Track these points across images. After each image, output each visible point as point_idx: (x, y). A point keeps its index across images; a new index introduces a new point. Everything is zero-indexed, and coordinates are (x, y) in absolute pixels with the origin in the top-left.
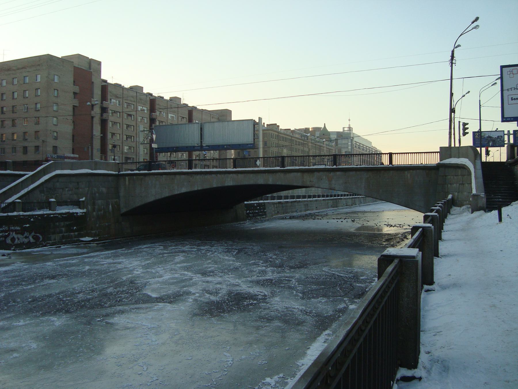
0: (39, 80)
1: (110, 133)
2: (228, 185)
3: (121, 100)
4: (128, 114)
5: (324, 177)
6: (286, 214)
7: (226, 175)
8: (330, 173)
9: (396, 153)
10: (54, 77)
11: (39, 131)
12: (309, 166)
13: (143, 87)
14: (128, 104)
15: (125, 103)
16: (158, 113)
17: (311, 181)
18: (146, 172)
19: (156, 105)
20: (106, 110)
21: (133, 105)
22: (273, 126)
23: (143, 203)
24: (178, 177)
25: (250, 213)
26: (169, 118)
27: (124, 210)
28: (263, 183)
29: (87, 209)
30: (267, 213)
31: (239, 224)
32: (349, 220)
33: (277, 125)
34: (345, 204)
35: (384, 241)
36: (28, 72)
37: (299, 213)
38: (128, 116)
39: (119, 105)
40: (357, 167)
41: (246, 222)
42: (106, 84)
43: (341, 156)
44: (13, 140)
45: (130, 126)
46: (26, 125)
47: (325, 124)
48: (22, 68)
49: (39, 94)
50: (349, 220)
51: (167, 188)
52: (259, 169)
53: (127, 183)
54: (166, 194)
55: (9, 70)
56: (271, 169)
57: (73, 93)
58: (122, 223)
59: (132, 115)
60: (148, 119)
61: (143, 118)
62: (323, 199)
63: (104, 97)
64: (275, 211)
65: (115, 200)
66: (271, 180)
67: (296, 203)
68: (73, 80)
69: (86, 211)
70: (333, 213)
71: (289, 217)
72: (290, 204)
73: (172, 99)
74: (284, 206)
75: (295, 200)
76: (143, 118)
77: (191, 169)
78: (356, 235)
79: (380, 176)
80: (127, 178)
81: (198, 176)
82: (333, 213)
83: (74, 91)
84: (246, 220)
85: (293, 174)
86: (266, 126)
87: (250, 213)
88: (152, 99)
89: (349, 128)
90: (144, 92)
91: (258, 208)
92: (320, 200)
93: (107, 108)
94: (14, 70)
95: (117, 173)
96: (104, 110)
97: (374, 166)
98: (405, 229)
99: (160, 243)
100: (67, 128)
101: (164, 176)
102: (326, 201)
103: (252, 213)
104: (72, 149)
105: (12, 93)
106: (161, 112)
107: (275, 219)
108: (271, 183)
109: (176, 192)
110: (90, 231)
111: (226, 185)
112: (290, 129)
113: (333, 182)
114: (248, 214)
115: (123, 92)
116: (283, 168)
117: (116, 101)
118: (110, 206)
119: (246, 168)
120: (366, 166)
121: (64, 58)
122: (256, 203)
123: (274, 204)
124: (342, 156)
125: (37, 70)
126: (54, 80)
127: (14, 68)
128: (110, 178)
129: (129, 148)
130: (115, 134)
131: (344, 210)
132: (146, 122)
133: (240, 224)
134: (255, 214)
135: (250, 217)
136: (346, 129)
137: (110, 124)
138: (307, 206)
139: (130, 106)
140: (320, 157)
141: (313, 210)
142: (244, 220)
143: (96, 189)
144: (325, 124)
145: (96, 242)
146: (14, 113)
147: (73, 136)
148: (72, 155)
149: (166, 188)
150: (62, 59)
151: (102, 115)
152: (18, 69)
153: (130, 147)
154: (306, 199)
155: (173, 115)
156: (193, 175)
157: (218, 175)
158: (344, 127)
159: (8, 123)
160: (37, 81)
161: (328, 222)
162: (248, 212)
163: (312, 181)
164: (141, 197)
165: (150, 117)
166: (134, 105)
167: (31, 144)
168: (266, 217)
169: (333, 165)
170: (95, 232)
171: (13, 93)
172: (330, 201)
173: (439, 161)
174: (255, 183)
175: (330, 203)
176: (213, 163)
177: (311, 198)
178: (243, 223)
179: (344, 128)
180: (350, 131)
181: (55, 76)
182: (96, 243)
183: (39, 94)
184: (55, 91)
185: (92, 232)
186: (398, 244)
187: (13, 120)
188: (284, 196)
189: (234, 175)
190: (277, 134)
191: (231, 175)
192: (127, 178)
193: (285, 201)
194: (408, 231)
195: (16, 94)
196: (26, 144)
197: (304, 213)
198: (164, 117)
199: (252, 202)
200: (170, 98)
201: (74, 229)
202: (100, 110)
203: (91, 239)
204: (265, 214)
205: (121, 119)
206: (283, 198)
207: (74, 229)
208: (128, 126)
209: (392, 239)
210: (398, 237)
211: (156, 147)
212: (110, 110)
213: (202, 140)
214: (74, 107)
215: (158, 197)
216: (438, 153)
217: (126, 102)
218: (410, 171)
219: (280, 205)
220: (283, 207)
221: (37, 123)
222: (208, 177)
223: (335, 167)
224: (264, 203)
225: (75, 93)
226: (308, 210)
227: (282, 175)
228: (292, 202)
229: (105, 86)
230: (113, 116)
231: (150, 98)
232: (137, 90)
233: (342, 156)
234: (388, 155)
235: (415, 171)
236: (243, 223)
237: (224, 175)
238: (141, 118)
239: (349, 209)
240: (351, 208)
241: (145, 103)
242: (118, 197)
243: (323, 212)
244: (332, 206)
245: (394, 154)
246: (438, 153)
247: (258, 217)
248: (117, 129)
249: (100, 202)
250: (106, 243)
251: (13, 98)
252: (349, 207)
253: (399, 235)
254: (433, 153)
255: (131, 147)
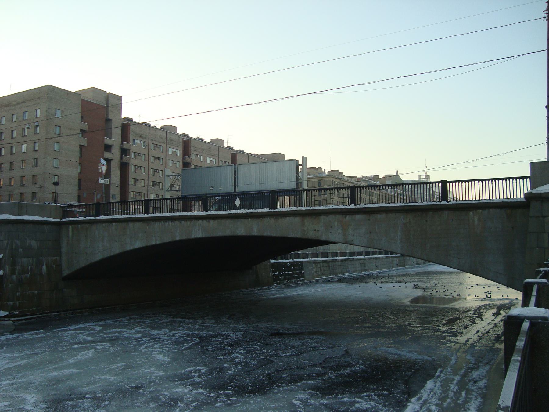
0: (38, 115)
1: (132, 178)
2: (196, 237)
3: (147, 141)
4: (155, 157)
5: (336, 223)
6: (335, 275)
7: (194, 222)
8: (345, 217)
9: (452, 182)
10: (56, 112)
11: (37, 175)
12: (312, 206)
13: (176, 127)
14: (156, 146)
15: (152, 145)
16: (193, 157)
17: (315, 230)
18: (93, 218)
19: (191, 147)
20: (128, 151)
21: (161, 147)
22: (335, 172)
23: (88, 263)
24: (131, 225)
25: (279, 275)
26: (208, 162)
27: (66, 273)
28: (244, 234)
29: (4, 270)
30: (305, 274)
31: (260, 289)
32: (410, 285)
33: (340, 171)
34: (415, 262)
35: (444, 325)
36: (28, 106)
37: (353, 275)
38: (155, 159)
39: (144, 146)
40: (388, 207)
41: (271, 287)
42: (188, 139)
43: (363, 189)
44: (11, 186)
45: (158, 171)
46: (24, 168)
47: (397, 171)
48: (24, 102)
49: (38, 132)
50: (410, 285)
51: (117, 241)
52: (239, 212)
53: (70, 234)
54: (116, 250)
55: (9, 105)
56: (255, 211)
57: (80, 130)
58: (65, 290)
59: (160, 158)
60: (181, 163)
61: (174, 162)
62: (387, 257)
63: (125, 137)
64: (318, 271)
65: (54, 258)
66: (255, 229)
67: (349, 262)
68: (80, 116)
69: (3, 273)
70: (397, 273)
71: (336, 280)
72: (340, 263)
73: (213, 141)
74: (330, 266)
75: (346, 258)
76: (174, 162)
77: (148, 214)
78: (406, 310)
79: (427, 221)
80: (70, 227)
81: (157, 224)
82: (397, 273)
83: (81, 129)
84: (271, 284)
85: (288, 220)
86: (326, 172)
87: (281, 276)
88: (185, 140)
89: (426, 175)
90: (178, 132)
91: (292, 268)
92: (382, 258)
93: (129, 150)
94: (14, 105)
95: (59, 220)
96: (124, 152)
97: (417, 204)
98: (482, 300)
99: (111, 321)
100: (74, 172)
101: (114, 224)
102: (390, 259)
103: (283, 275)
104: (77, 196)
105: (11, 131)
106: (197, 155)
107: (318, 282)
108: (256, 234)
109: (129, 248)
110: (6, 302)
111: (193, 237)
112: (355, 177)
113: (350, 231)
114: (277, 276)
115: (149, 132)
116: (272, 210)
117: (140, 142)
118: (44, 267)
119: (221, 210)
120: (404, 204)
121: (77, 93)
122: (289, 262)
123: (315, 263)
124: (364, 188)
125: (36, 104)
126: (56, 115)
127: (14, 103)
128: (46, 227)
129: (156, 196)
130: (139, 180)
131: (412, 270)
132: (178, 166)
133: (263, 289)
134: (287, 277)
135: (279, 279)
136: (422, 177)
137: (132, 169)
138: (363, 265)
139: (158, 147)
140: (330, 190)
141: (371, 270)
142: (270, 284)
143: (19, 243)
144: (397, 171)
145: (12, 319)
146: (12, 154)
147: (79, 180)
148: (77, 203)
149: (116, 241)
150: (77, 94)
151: (121, 158)
152: (18, 104)
153: (157, 196)
154: (363, 257)
155: (211, 159)
156: (151, 222)
157: (183, 222)
158: (421, 175)
159: (6, 166)
160: (36, 116)
161: (381, 288)
162: (277, 273)
163: (317, 230)
164: (86, 254)
165: (183, 161)
166: (163, 146)
167: (28, 191)
168: (303, 280)
169: (349, 204)
170: (13, 304)
171: (12, 131)
172: (395, 259)
173: (529, 189)
174: (232, 234)
175: (396, 261)
176: (171, 204)
177: (369, 256)
178: (267, 289)
179: (420, 176)
180: (427, 178)
181: (57, 110)
182: (13, 321)
183: (38, 132)
184: (56, 128)
185: (9, 303)
186: (464, 331)
187: (11, 163)
188: (358, 252)
189: (204, 222)
190: (339, 181)
191: (200, 221)
192: (70, 227)
193: (333, 260)
194: (485, 304)
195: (15, 132)
196: (23, 190)
197: (359, 274)
198: (201, 161)
199: (284, 261)
200: (211, 140)
201: (277, 272)
202: (120, 151)
203: (6, 313)
204: (303, 275)
205: (147, 162)
206: (330, 255)
207: (277, 272)
208: (155, 171)
209: (459, 319)
210: (468, 315)
211: (106, 183)
212: (133, 152)
213: (236, 185)
214: (81, 147)
215: (107, 254)
216: (528, 179)
217: (152, 143)
218: (478, 211)
219: (326, 265)
220: (329, 267)
221: (36, 165)
222: (170, 224)
223: (352, 206)
224: (302, 262)
225: (82, 131)
226: (365, 270)
227: (271, 221)
228: (342, 260)
229: (127, 124)
230: (136, 158)
231: (183, 139)
232: (169, 130)
233: (364, 188)
234: (440, 184)
235: (486, 212)
236: (267, 289)
237: (190, 223)
238: (172, 162)
239: (419, 269)
240: (423, 267)
241: (177, 145)
242: (60, 254)
243: (386, 272)
244: (397, 265)
245: (449, 182)
246: (528, 179)
247: (292, 280)
248: (141, 174)
249: (25, 260)
250: (32, 320)
251: (12, 138)
252: (420, 266)
253: (470, 312)
254: (518, 180)
255: (158, 195)
